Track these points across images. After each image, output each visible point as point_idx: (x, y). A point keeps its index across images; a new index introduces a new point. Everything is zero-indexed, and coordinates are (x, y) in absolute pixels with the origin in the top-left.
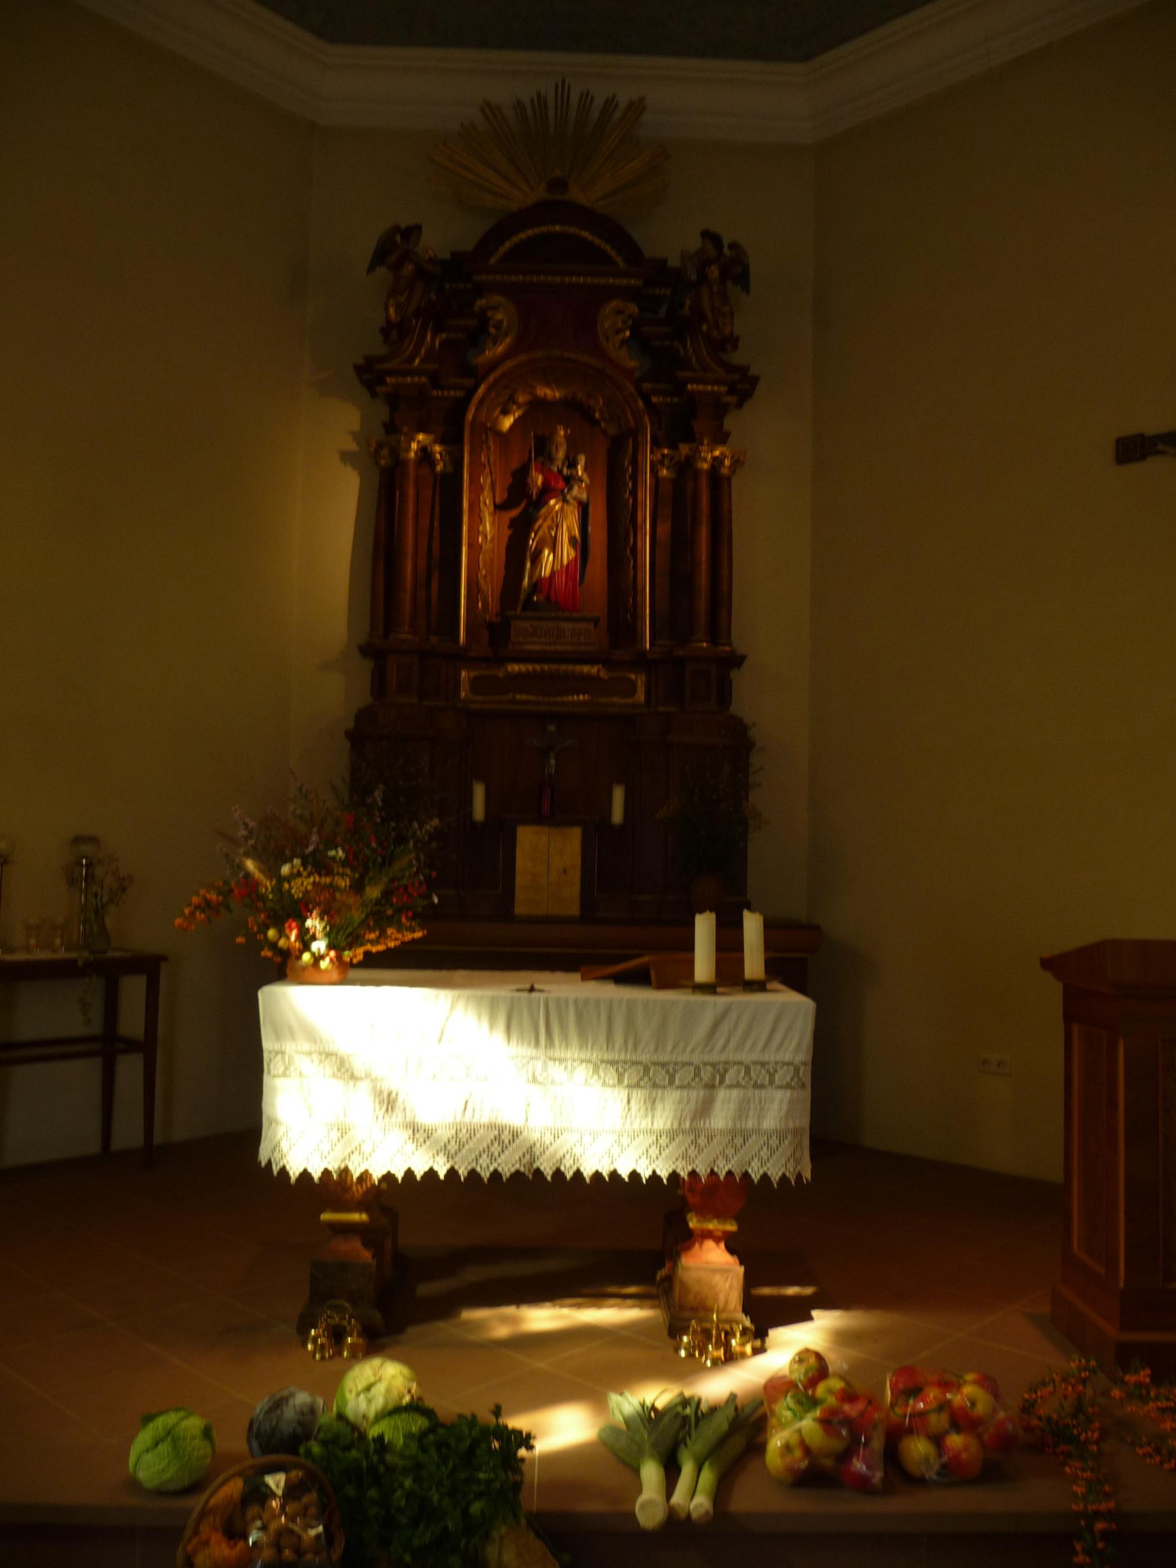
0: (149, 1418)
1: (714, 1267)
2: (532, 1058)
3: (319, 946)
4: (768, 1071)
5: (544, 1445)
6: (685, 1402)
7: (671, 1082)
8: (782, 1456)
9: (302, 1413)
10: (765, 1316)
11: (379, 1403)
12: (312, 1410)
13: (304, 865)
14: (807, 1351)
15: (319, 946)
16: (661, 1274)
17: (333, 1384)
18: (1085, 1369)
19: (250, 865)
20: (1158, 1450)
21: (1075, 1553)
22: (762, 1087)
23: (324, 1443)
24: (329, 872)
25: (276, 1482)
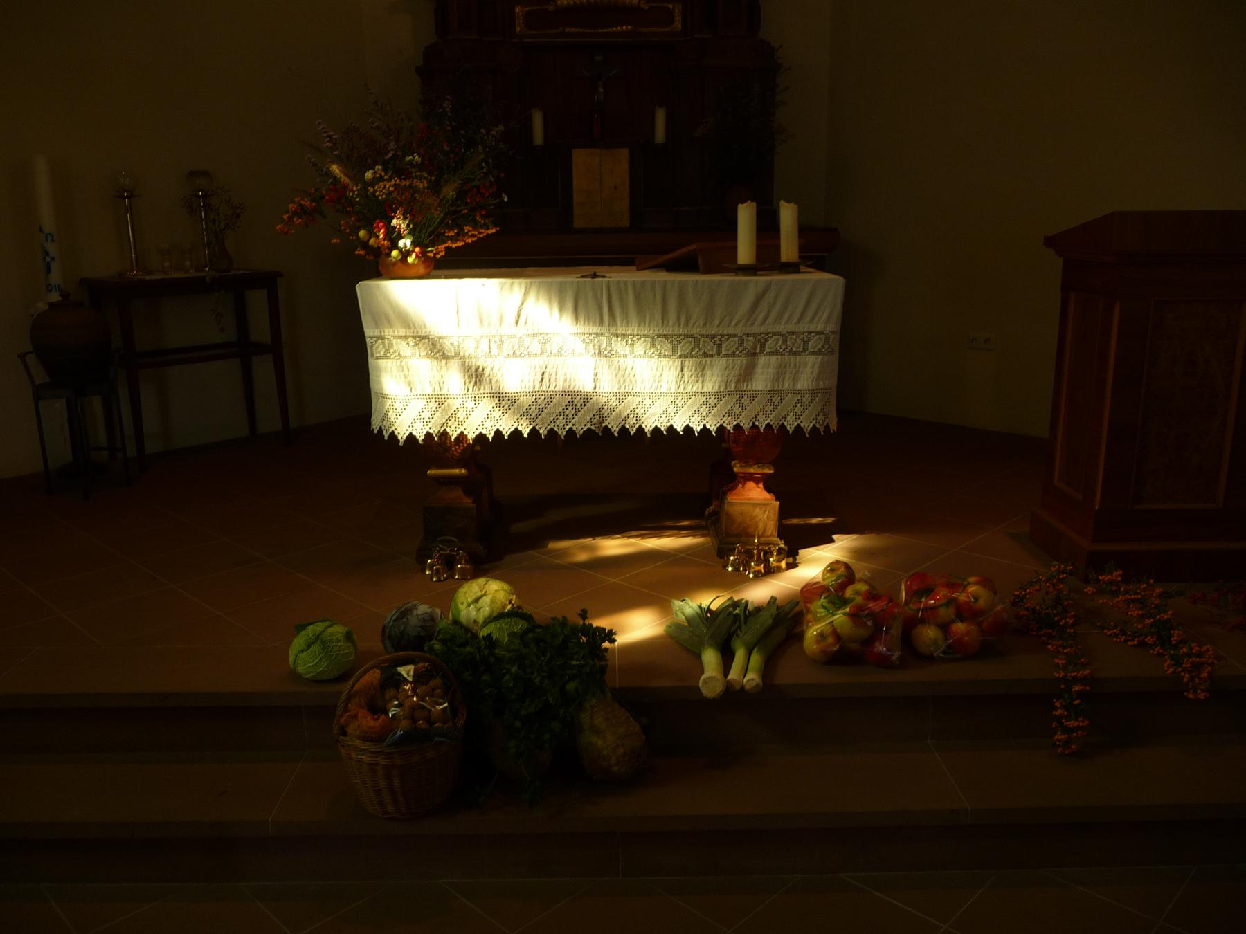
0: (302, 627)
1: (754, 502)
2: (598, 335)
3: (405, 243)
4: (802, 340)
5: (622, 639)
6: (735, 604)
7: (719, 352)
8: (818, 642)
9: (425, 621)
10: (795, 541)
11: (486, 611)
12: (432, 618)
13: (385, 170)
14: (837, 562)
15: (405, 243)
16: (709, 510)
17: (448, 599)
18: (1063, 572)
19: (335, 169)
20: (1123, 632)
21: (1056, 709)
22: (797, 353)
23: (444, 642)
24: (408, 176)
25: (407, 671)
